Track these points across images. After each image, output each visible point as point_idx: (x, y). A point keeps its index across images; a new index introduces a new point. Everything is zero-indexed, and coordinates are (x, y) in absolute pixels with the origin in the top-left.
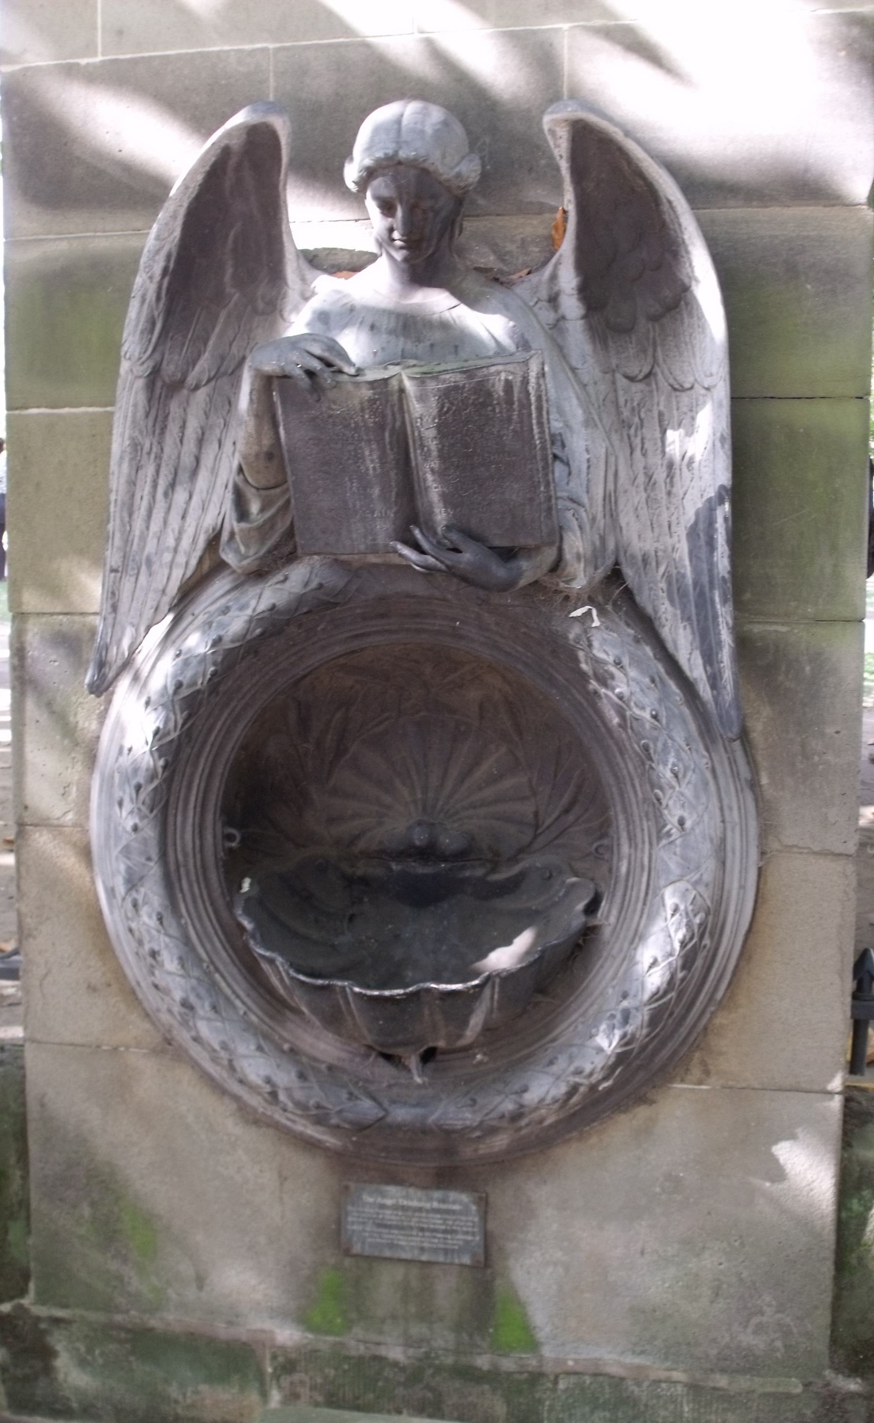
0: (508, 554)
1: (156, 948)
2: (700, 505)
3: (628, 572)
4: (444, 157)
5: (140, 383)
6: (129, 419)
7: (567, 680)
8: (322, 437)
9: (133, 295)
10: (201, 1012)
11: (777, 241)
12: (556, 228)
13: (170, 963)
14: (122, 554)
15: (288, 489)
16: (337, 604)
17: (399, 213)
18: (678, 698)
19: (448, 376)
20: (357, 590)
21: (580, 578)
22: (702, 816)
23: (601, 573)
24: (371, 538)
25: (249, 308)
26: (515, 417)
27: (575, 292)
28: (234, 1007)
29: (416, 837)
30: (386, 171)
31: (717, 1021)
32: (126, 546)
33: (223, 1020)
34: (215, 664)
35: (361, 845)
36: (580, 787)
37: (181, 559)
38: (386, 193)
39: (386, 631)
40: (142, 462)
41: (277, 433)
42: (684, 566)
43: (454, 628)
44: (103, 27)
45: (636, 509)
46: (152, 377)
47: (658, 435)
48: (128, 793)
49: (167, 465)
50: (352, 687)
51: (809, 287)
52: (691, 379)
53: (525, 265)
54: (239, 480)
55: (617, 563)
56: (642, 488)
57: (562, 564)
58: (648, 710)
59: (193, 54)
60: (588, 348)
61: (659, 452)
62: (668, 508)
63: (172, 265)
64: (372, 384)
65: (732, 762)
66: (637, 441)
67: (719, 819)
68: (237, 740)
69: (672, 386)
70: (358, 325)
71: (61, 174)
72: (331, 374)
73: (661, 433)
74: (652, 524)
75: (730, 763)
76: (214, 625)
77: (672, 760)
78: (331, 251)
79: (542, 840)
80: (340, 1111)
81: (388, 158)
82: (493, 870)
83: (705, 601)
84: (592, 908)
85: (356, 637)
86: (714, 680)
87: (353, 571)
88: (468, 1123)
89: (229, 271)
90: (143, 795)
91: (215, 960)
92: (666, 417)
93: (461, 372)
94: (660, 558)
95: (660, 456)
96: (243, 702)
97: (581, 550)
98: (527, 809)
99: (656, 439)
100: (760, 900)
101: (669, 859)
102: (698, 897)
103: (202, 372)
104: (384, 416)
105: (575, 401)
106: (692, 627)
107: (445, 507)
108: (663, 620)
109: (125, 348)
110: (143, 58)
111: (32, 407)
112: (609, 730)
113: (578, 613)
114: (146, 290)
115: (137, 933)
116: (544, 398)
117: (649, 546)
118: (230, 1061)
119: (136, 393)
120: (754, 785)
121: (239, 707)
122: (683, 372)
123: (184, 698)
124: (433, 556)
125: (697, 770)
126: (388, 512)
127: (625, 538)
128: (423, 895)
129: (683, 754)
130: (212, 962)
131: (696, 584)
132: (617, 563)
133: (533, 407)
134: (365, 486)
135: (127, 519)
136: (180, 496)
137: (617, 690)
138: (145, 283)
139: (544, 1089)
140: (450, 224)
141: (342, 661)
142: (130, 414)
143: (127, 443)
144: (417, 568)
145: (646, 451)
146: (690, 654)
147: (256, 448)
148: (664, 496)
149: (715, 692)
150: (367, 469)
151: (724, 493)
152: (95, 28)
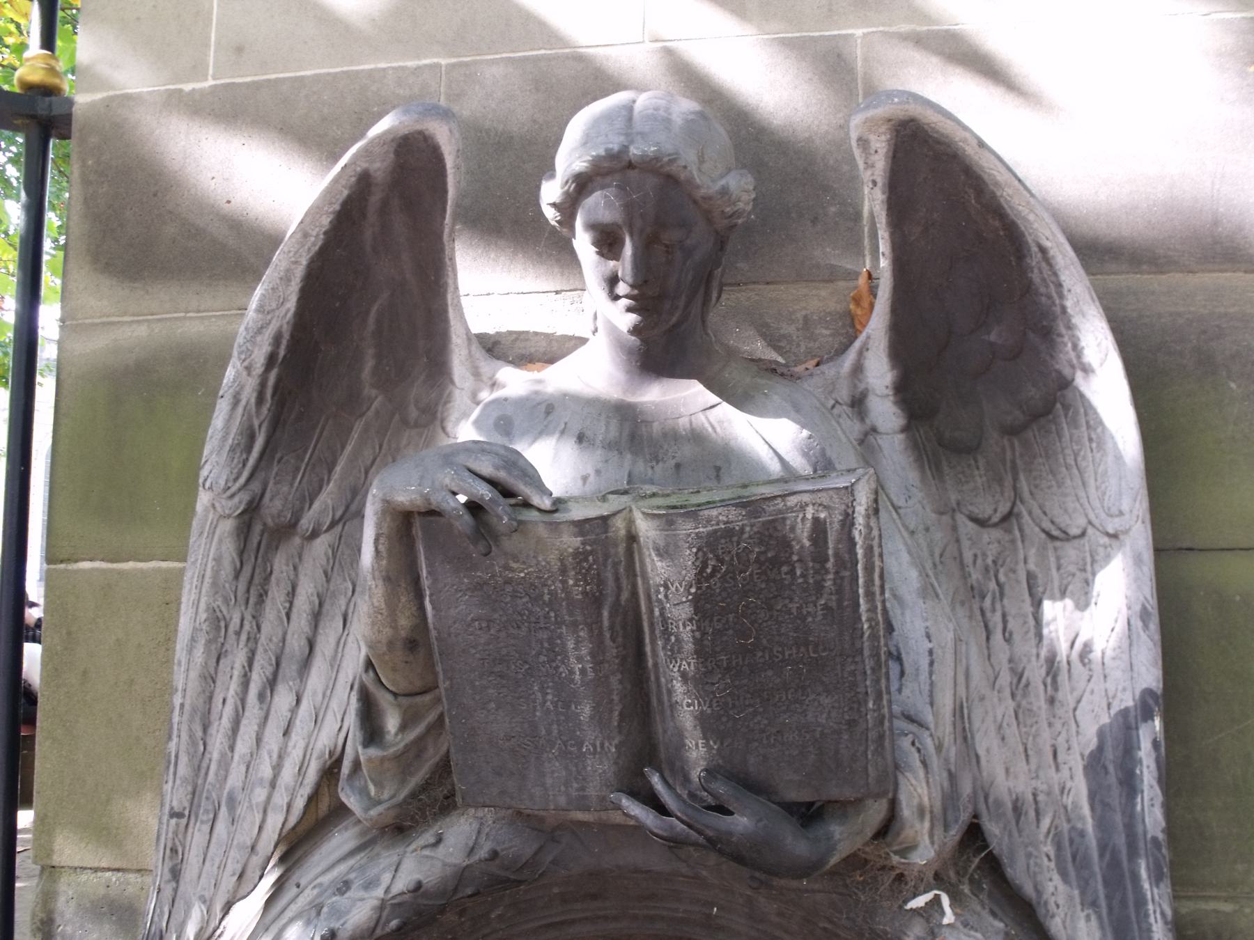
0: (809, 815)
2: (1105, 719)
3: (992, 828)
4: (701, 160)
5: (228, 526)
6: (208, 580)
8: (496, 616)
9: (221, 393)
11: (1181, 321)
12: (857, 301)
14: (190, 788)
15: (438, 700)
16: (520, 882)
17: (628, 250)
19: (714, 512)
20: (552, 862)
21: (925, 847)
23: (955, 833)
25: (397, 417)
26: (828, 583)
27: (890, 392)
30: (608, 180)
32: (197, 776)
37: (281, 799)
38: (608, 215)
40: (227, 646)
41: (422, 608)
42: (1082, 818)
43: (709, 916)
44: (218, 43)
45: (1000, 727)
46: (246, 517)
47: (1028, 608)
49: (266, 651)
51: (1233, 385)
52: (1082, 521)
53: (810, 354)
54: (368, 679)
55: (976, 816)
56: (1007, 693)
59: (336, 74)
60: (913, 476)
61: (1032, 634)
62: (1050, 725)
63: (282, 352)
64: (581, 526)
66: (996, 619)
69: (1048, 534)
70: (557, 435)
71: (155, 237)
72: (508, 509)
73: (1032, 605)
74: (1026, 750)
76: (325, 910)
78: (519, 336)
81: (612, 156)
83: (1122, 876)
87: (546, 830)
89: (369, 364)
92: (1040, 581)
93: (736, 505)
94: (1042, 805)
95: (1033, 642)
97: (926, 800)
99: (1025, 616)
103: (323, 511)
104: (601, 582)
105: (905, 557)
106: (1100, 918)
107: (705, 738)
108: (1052, 906)
109: (204, 473)
110: (269, 80)
111: (84, 560)
113: (919, 902)
114: (242, 387)
116: (876, 550)
117: (1022, 785)
119: (220, 541)
122: (1066, 511)
126: (607, 744)
127: (985, 774)
131: (1103, 848)
132: (976, 816)
133: (860, 567)
134: (567, 700)
135: (199, 734)
136: (283, 700)
138: (239, 376)
140: (705, 284)
142: (209, 573)
143: (203, 616)
145: (1011, 634)
147: (388, 632)
148: (1042, 703)
150: (572, 672)
151: (1151, 702)
152: (207, 46)
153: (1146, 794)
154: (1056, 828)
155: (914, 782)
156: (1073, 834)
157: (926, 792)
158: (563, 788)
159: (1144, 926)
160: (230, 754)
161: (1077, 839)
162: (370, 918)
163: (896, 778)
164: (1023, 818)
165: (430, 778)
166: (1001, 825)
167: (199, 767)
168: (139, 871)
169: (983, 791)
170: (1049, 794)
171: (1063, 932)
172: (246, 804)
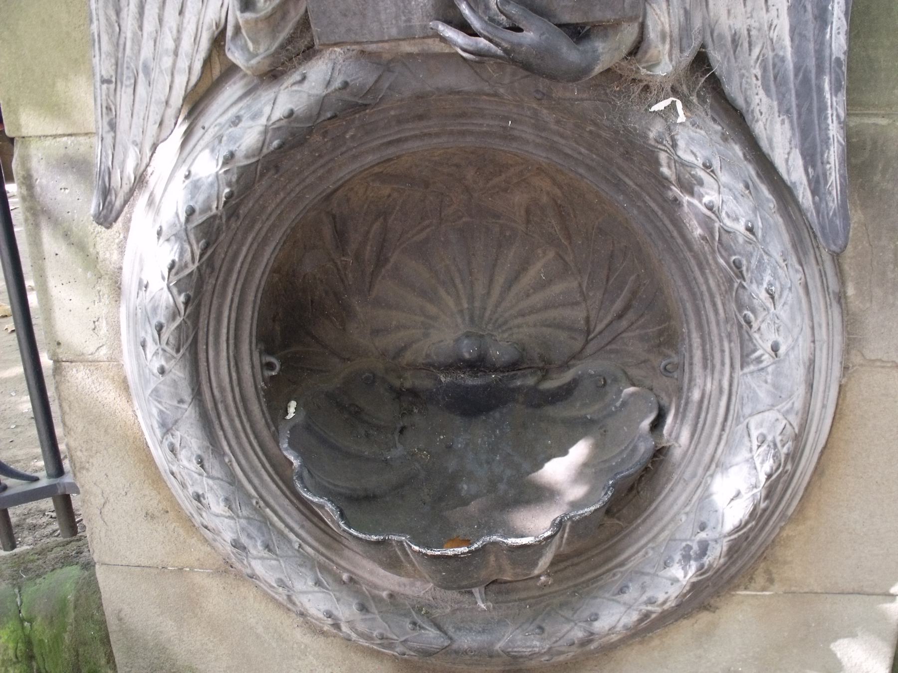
1: (200, 492)
3: (715, 56)
7: (639, 186)
10: (253, 552)
13: (217, 506)
14: (113, 61)
16: (366, 106)
18: (772, 206)
20: (389, 88)
21: (665, 63)
22: (797, 340)
23: (688, 56)
24: (403, 18)
28: (290, 541)
29: (464, 350)
31: (784, 534)
32: (117, 50)
33: (277, 557)
34: (229, 184)
35: (408, 356)
36: (634, 293)
39: (425, 135)
42: (783, 48)
43: (505, 128)
48: (149, 334)
50: (389, 196)
55: (703, 46)
57: (644, 46)
58: (743, 222)
65: (823, 274)
67: (809, 339)
68: (267, 264)
75: (821, 276)
76: (225, 138)
77: (767, 278)
79: (591, 348)
80: (405, 641)
82: (544, 378)
83: (810, 89)
84: (657, 425)
85: (390, 143)
86: (817, 185)
87: (384, 64)
88: (537, 650)
90: (167, 334)
91: (264, 494)
94: (754, 39)
96: (270, 223)
98: (578, 315)
100: (838, 416)
101: (754, 385)
102: (788, 426)
106: (791, 122)
108: (757, 114)
112: (688, 242)
113: (660, 106)
115: (179, 477)
117: (740, 24)
118: (289, 597)
120: (841, 298)
121: (265, 230)
123: (197, 227)
124: (486, 37)
125: (793, 289)
127: (712, 14)
128: (473, 405)
129: (780, 271)
130: (261, 497)
131: (797, 69)
132: (703, 46)
135: (114, 18)
137: (706, 199)
139: (615, 619)
141: (377, 170)
144: (465, 55)
146: (789, 154)
149: (817, 198)
153: (834, 24)
154: (764, 56)
155: (658, 11)
156: (776, 60)
157: (667, 20)
158: (394, 22)
159: (823, 126)
160: (140, 33)
161: (779, 64)
162: (258, 140)
163: (645, 9)
164: (739, 48)
165: (294, 33)
166: (723, 53)
167: (118, 44)
168: (86, 134)
169: (710, 27)
170: (759, 30)
171: (764, 132)
172: (158, 70)
